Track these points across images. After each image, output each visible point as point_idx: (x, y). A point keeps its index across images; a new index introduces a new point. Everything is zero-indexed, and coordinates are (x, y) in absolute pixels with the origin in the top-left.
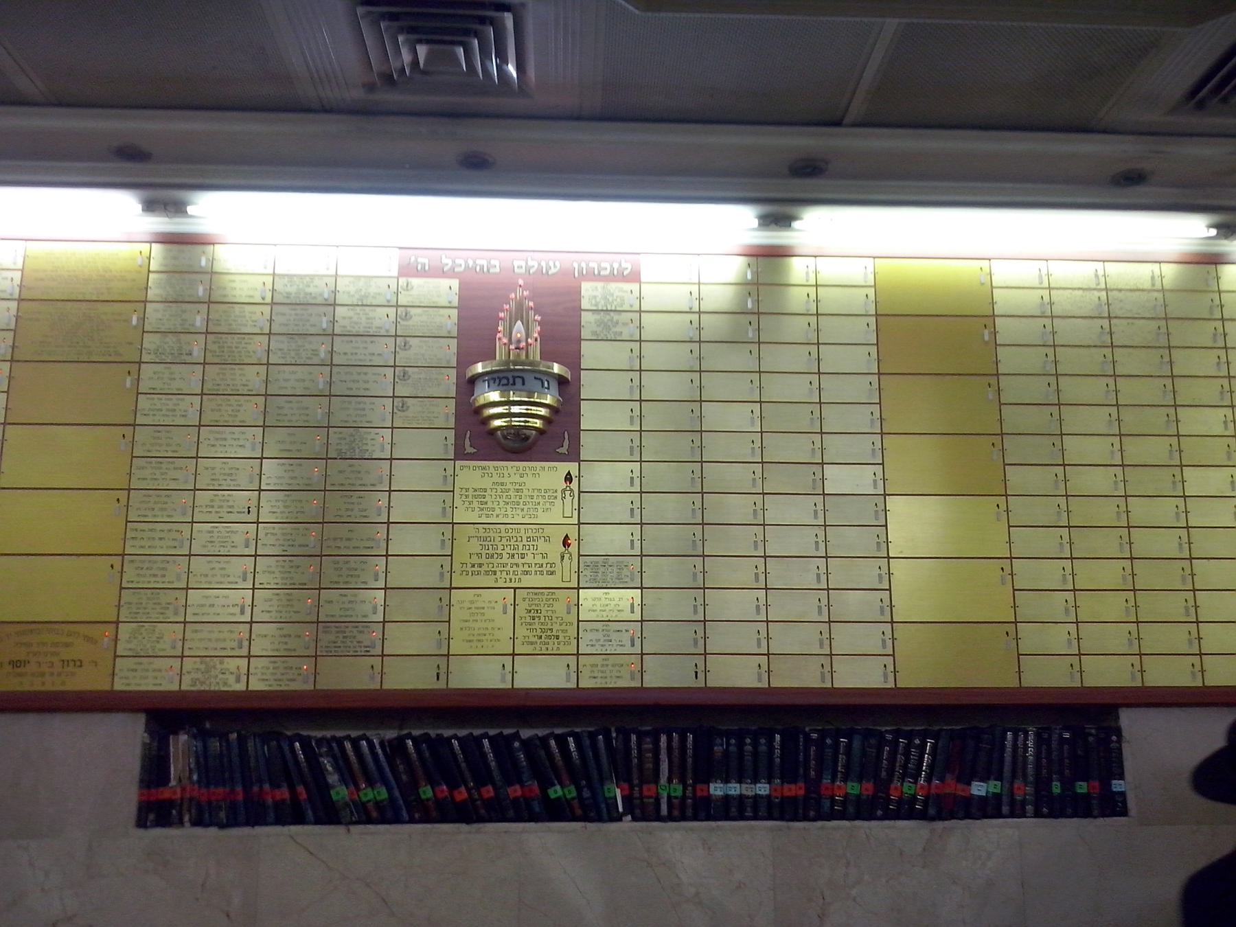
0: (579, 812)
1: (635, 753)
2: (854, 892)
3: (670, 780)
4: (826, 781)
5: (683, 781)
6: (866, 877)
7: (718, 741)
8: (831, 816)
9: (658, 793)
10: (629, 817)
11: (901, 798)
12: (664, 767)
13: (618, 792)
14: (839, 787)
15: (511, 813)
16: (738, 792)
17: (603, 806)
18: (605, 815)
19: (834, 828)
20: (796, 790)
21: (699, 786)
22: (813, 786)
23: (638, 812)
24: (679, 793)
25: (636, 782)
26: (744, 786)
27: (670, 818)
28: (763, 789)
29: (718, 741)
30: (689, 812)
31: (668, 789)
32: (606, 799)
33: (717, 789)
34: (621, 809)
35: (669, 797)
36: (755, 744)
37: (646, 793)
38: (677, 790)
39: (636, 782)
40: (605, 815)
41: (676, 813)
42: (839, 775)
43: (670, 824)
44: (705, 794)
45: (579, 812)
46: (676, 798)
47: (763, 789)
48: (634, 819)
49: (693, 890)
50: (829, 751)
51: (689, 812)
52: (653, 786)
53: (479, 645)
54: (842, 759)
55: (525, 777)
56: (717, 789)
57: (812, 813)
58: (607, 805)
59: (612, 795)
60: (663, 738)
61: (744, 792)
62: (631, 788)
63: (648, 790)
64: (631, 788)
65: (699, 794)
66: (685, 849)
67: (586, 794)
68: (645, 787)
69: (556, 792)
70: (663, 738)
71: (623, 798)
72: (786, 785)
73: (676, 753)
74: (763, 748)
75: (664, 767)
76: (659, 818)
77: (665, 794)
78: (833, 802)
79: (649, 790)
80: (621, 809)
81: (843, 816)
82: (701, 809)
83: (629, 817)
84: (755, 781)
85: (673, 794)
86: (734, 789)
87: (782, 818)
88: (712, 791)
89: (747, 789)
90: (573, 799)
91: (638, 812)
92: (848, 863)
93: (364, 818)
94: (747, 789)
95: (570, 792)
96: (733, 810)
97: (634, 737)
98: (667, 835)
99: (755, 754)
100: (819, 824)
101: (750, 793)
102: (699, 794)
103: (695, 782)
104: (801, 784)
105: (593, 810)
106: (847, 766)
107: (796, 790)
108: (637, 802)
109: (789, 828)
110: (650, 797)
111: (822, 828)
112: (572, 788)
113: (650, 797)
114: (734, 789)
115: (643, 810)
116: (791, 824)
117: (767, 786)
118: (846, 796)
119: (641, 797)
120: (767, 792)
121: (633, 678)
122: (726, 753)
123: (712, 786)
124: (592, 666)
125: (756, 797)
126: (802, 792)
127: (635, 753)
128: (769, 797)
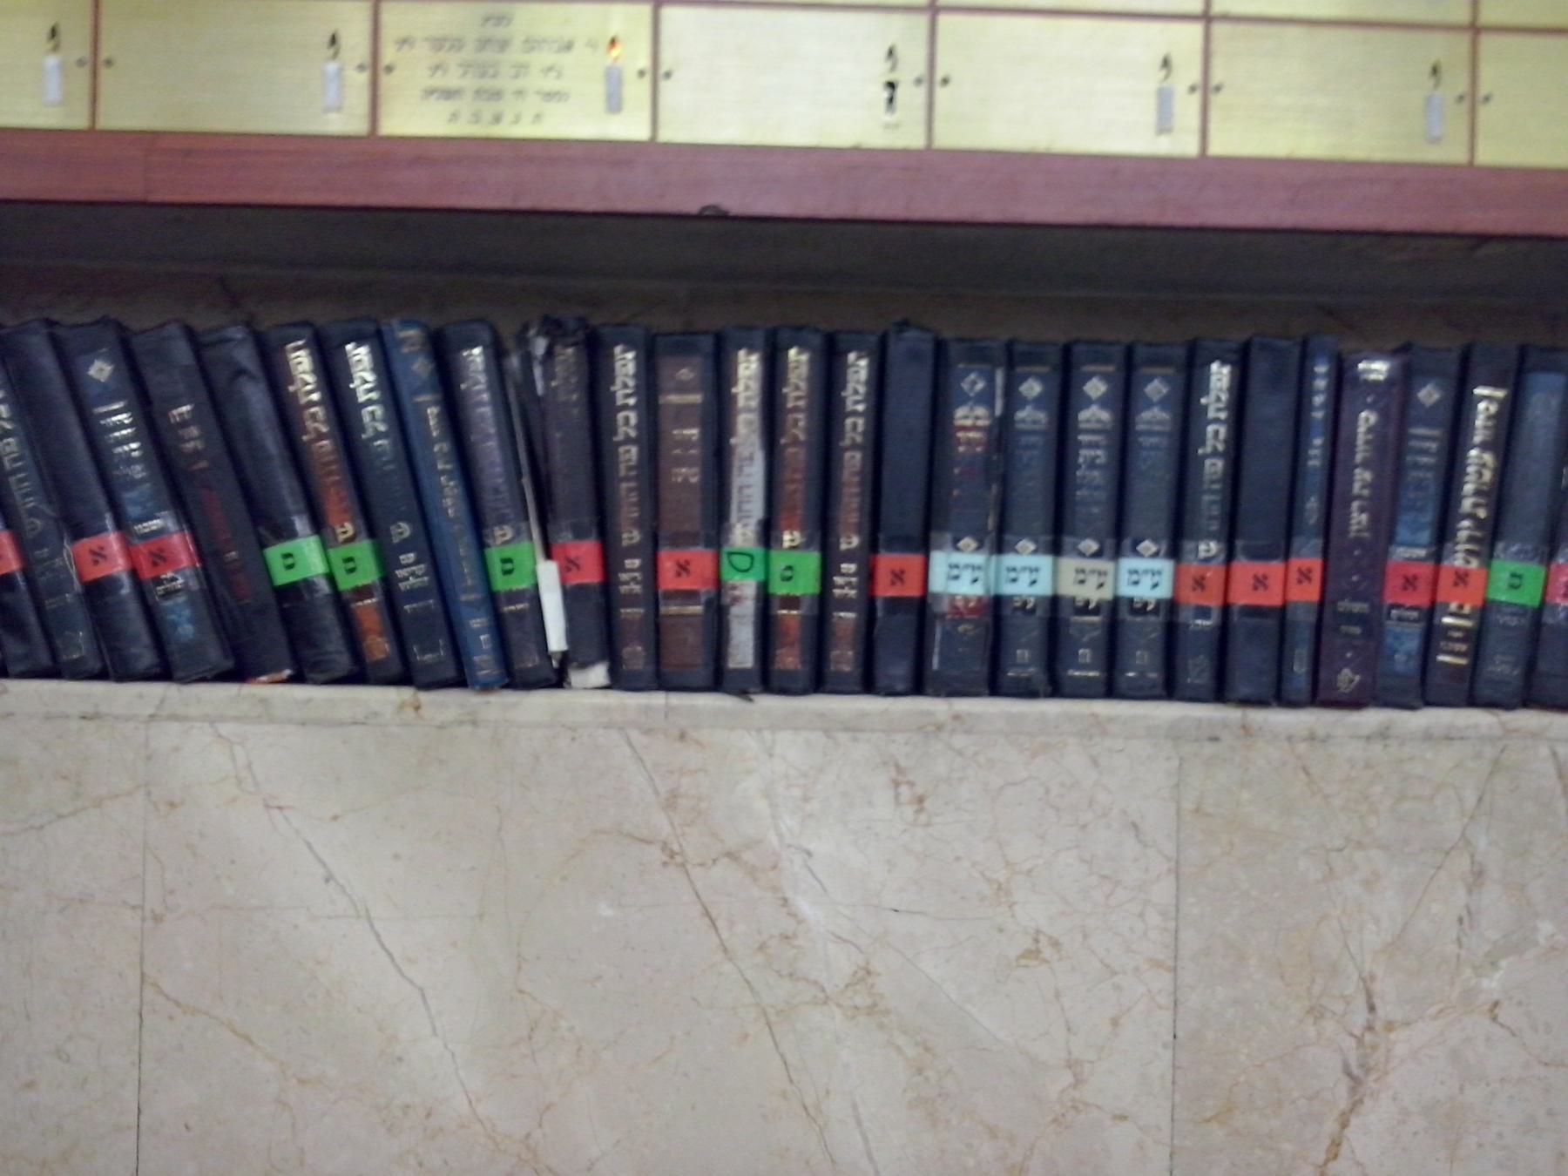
0: (379, 647)
1: (627, 422)
2: (1492, 984)
3: (768, 533)
4: (1409, 552)
5: (823, 534)
6: (1546, 928)
7: (974, 383)
8: (1424, 689)
9: (719, 583)
10: (599, 674)
12: (749, 479)
13: (548, 576)
14: (1461, 577)
15: (80, 643)
16: (1044, 588)
17: (477, 624)
18: (483, 656)
19: (1427, 736)
20: (1289, 582)
21: (887, 561)
22: (1355, 568)
23: (635, 654)
24: (805, 583)
25: (631, 536)
26: (1069, 564)
27: (766, 679)
28: (1145, 577)
29: (974, 383)
30: (844, 658)
31: (763, 565)
32: (493, 600)
33: (958, 574)
34: (557, 640)
35: (765, 600)
36: (1125, 402)
37: (669, 579)
38: (797, 570)
39: (631, 536)
40: (483, 656)
41: (789, 659)
42: (1465, 528)
43: (769, 704)
44: (912, 591)
45: (379, 647)
46: (791, 602)
47: (1145, 577)
48: (619, 680)
49: (843, 963)
50: (1427, 440)
51: (844, 658)
52: (699, 556)
54: (1479, 463)
55: (132, 501)
56: (958, 574)
57: (1347, 678)
58: (499, 626)
59: (519, 583)
60: (748, 367)
61: (1069, 589)
62: (609, 561)
63: (681, 568)
64: (609, 561)
65: (885, 589)
66: (814, 791)
67: (412, 573)
68: (668, 560)
69: (303, 558)
70: (748, 367)
71: (572, 597)
72: (1245, 569)
73: (799, 425)
74: (1154, 418)
75: (749, 479)
76: (718, 679)
77: (745, 587)
78: (1432, 635)
79: (683, 568)
80: (557, 640)
81: (1469, 691)
82: (901, 651)
83: (599, 674)
84: (1118, 540)
85: (779, 589)
86: (1029, 574)
87: (1219, 693)
88: (939, 582)
89: (1082, 577)
90: (363, 592)
91: (635, 654)
92: (1478, 875)
94: (1082, 577)
95: (350, 564)
96: (1023, 654)
97: (626, 363)
98: (749, 742)
99: (1123, 436)
100: (1372, 718)
101: (1091, 593)
102: (885, 589)
103: (872, 545)
104: (1308, 558)
105: (432, 641)
106: (1499, 495)
107: (1289, 582)
108: (631, 613)
109: (1245, 728)
110: (690, 596)
111: (1383, 734)
112: (363, 551)
113: (690, 596)
114: (1029, 574)
115: (651, 645)
116: (1257, 716)
117: (1166, 566)
118: (1485, 610)
119: (653, 596)
120: (1164, 591)
121: (614, 103)
122: (1002, 433)
123: (940, 561)
124: (438, 43)
125: (1116, 611)
126: (1309, 593)
127: (627, 422)
128: (1171, 607)
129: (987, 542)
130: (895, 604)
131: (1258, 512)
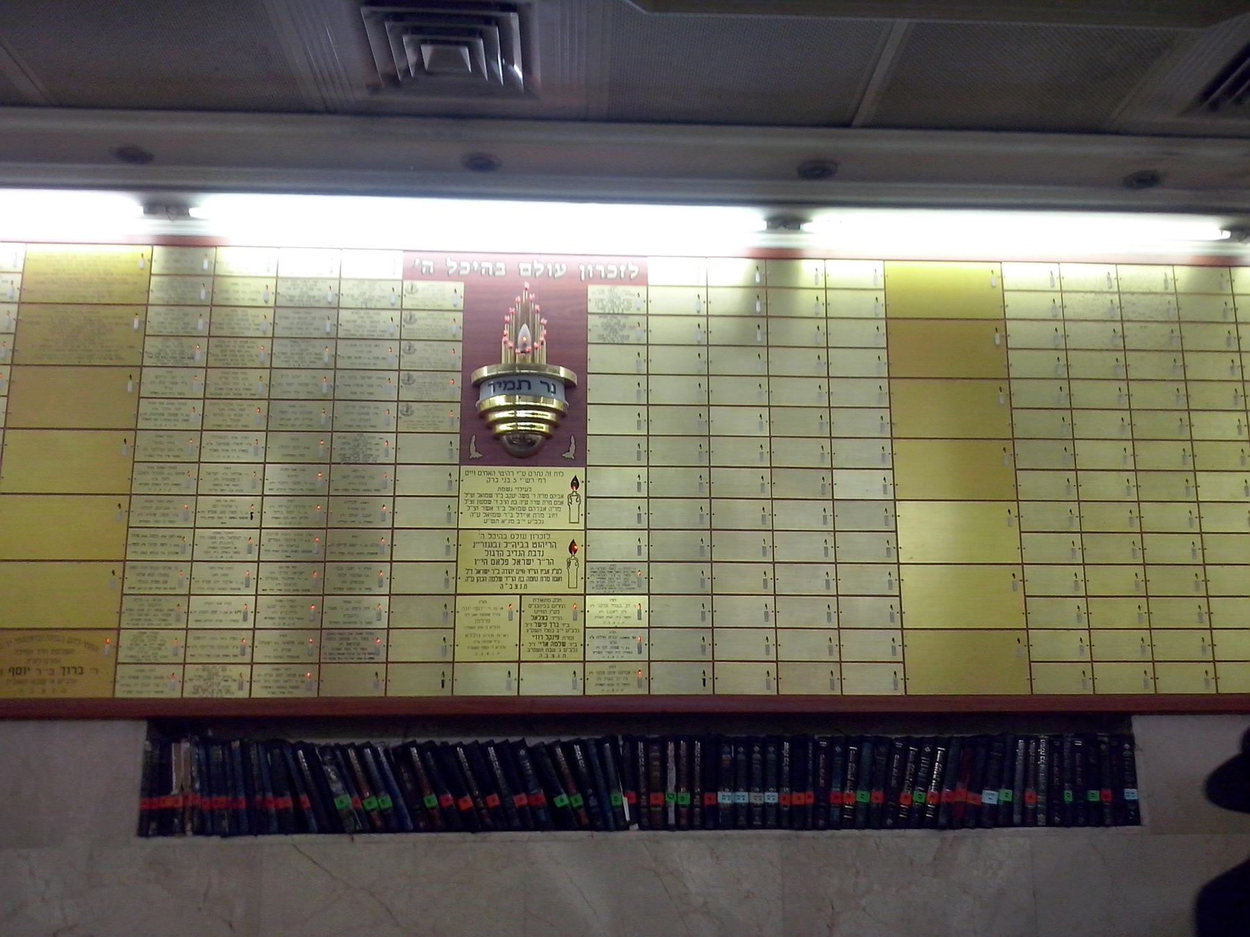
0: (585, 821)
1: (642, 761)
2: (864, 902)
3: (677, 789)
4: (836, 789)
5: (690, 789)
6: (876, 887)
7: (726, 749)
8: (841, 825)
9: (665, 802)
10: (636, 826)
11: (911, 807)
12: (672, 775)
13: (625, 800)
14: (849, 796)
15: (517, 822)
16: (746, 801)
17: (610, 814)
18: (612, 824)
19: (843, 837)
20: (805, 798)
21: (707, 795)
22: (823, 795)
23: (645, 820)
24: (687, 802)
25: (643, 790)
26: (752, 794)
27: (678, 827)
28: (771, 797)
29: (726, 749)
30: (697, 821)
31: (676, 797)
32: (613, 807)
33: (725, 798)
34: (628, 818)
35: (677, 806)
36: (764, 752)
37: (653, 802)
38: (685, 798)
39: (643, 790)
40: (612, 824)
41: (684, 822)
42: (849, 784)
43: (678, 833)
44: (713, 802)
45: (585, 821)
46: (684, 806)
47: (771, 797)
48: (642, 828)
49: (700, 900)
50: (838, 760)
51: (697, 821)
52: (660, 795)
53: (485, 652)
54: (851, 767)
55: (531, 785)
56: (725, 798)
57: (821, 822)
58: (614, 813)
59: (619, 803)
60: (671, 746)
61: (753, 801)
62: (639, 796)
63: (656, 798)
64: (639, 796)
65: (707, 802)
66: (693, 858)
67: (593, 802)
68: (652, 796)
69: (562, 800)
70: (671, 746)
71: (630, 806)
72: (795, 794)
73: (684, 761)
74: (772, 756)
75: (672, 775)
76: (666, 827)
77: (673, 803)
78: (843, 810)
79: (656, 798)
80: (628, 818)
81: (852, 825)
82: (709, 818)
83: (636, 826)
84: (764, 789)
85: (680, 803)
86: (743, 797)
87: (790, 827)
88: (720, 800)
89: (756, 798)
90: (580, 807)
91: (645, 820)
92: (858, 873)
93: (368, 826)
94: (756, 798)
95: (576, 801)
96: (742, 818)
97: (641, 745)
98: (675, 844)
99: (764, 762)
100: (829, 832)
101: (758, 802)
102: (707, 802)
103: (703, 791)
104: (810, 793)
105: (600, 819)
106: (857, 774)
107: (805, 798)
108: (644, 810)
109: (798, 837)
110: (658, 806)
111: (832, 837)
112: (579, 796)
113: (658, 806)
114: (743, 797)
115: (650, 819)
116: (800, 833)
117: (776, 794)
118: (856, 804)
119: (649, 806)
120: (776, 801)
121: (640, 686)
122: (734, 761)
123: (720, 794)
124: (599, 673)
125: (765, 805)
126: (811, 801)
127: (642, 761)
128: (777, 805)
129: (605, 333)
130: (656, 791)
131: (798, 783)
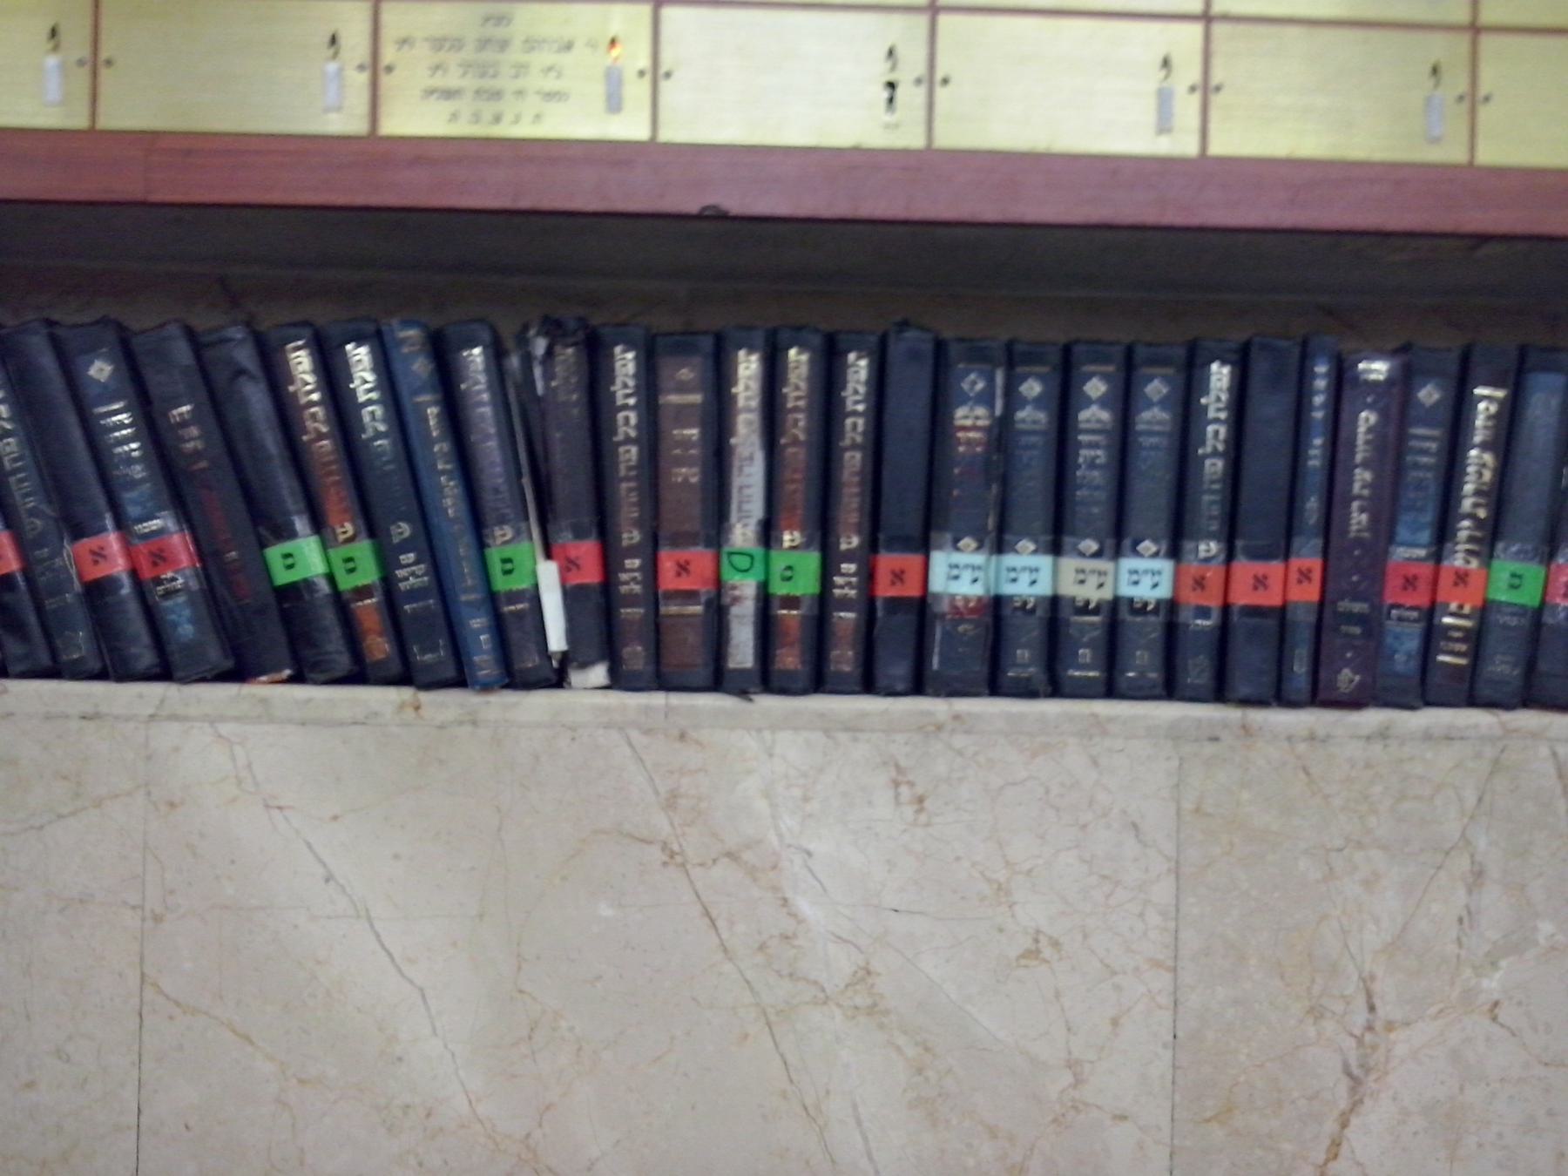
0: (379, 647)
1: (627, 422)
2: (1492, 984)
3: (768, 533)
4: (1409, 552)
5: (823, 534)
6: (1546, 928)
7: (974, 383)
8: (1424, 689)
9: (719, 583)
10: (599, 674)
11: (1485, 610)
12: (749, 479)
13: (548, 576)
14: (1461, 577)
15: (80, 643)
16: (1044, 588)
17: (477, 624)
18: (483, 656)
19: (1427, 736)
20: (1289, 582)
21: (887, 561)
22: (1355, 568)
23: (635, 654)
24: (805, 583)
25: (631, 536)
26: (1069, 564)
27: (766, 679)
28: (1145, 577)
29: (974, 383)
30: (844, 658)
31: (763, 565)
32: (493, 600)
33: (958, 574)
34: (557, 640)
35: (765, 600)
36: (1125, 402)
37: (669, 579)
38: (797, 570)
39: (631, 536)
40: (483, 656)
41: (789, 659)
42: (1465, 528)
43: (769, 704)
44: (912, 591)
45: (379, 647)
46: (791, 602)
47: (1145, 577)
48: (619, 680)
49: (843, 963)
50: (1427, 440)
51: (844, 658)
52: (699, 556)
53: (488, 109)
54: (1479, 463)
55: (132, 501)
56: (958, 574)
57: (1347, 678)
58: (499, 626)
59: (519, 583)
60: (748, 367)
61: (1069, 589)
62: (609, 561)
63: (681, 568)
64: (609, 561)
65: (885, 589)
66: (814, 791)
67: (412, 573)
68: (668, 560)
69: (303, 558)
70: (748, 367)
71: (572, 597)
72: (1245, 569)
73: (799, 425)
74: (1154, 418)
75: (749, 479)
76: (718, 679)
77: (745, 587)
78: (1432, 635)
79: (683, 568)
80: (557, 640)
81: (1469, 691)
82: (901, 651)
83: (599, 674)
84: (1118, 540)
85: (779, 589)
86: (1029, 574)
87: (1219, 693)
88: (939, 582)
89: (1082, 577)
90: (363, 592)
91: (635, 654)
92: (1478, 875)
93: (45, 659)
94: (1082, 577)
95: (350, 564)
96: (1023, 654)
97: (626, 363)
98: (749, 742)
99: (1123, 436)
100: (1372, 718)
101: (1091, 593)
102: (885, 589)
103: (872, 545)
104: (1308, 558)
105: (432, 641)
106: (1499, 495)
107: (1289, 582)
108: (631, 613)
109: (1245, 728)
110: (690, 596)
111: (1383, 734)
112: (363, 551)
113: (690, 596)
114: (1029, 574)
115: (651, 645)
116: (1257, 716)
117: (1166, 566)
118: (1485, 610)
119: (653, 596)
120: (1164, 591)
121: (614, 103)
122: (1002, 433)
123: (940, 561)
124: (438, 43)
125: (1116, 611)
126: (1309, 593)
127: (627, 422)
128: (1171, 607)
